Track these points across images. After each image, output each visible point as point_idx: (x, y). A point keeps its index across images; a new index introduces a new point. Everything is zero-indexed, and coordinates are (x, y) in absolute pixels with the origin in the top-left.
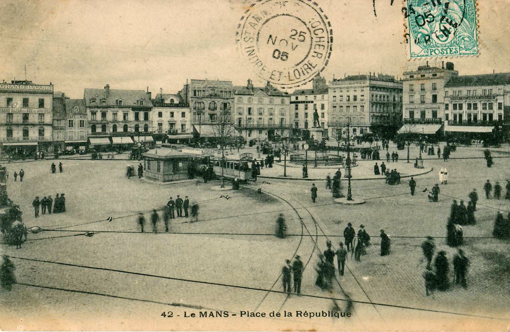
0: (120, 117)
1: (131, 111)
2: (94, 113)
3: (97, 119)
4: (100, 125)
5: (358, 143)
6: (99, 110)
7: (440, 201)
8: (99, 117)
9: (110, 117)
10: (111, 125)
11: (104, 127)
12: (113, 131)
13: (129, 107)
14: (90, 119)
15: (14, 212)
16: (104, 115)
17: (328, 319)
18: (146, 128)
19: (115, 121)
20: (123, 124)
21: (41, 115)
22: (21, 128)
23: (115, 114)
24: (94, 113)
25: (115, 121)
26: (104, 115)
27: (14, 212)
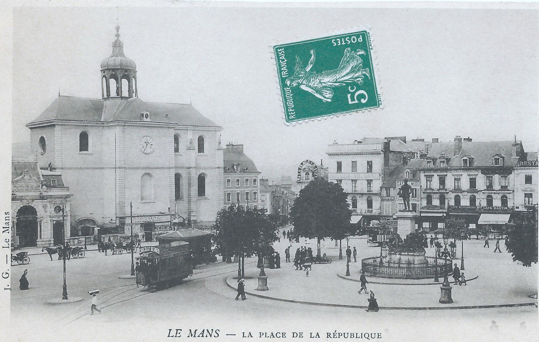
0: (465, 184)
1: (480, 174)
2: (429, 178)
3: (432, 187)
4: (437, 196)
5: (267, 211)
6: (435, 174)
7: (31, 288)
8: (435, 184)
9: (450, 183)
10: (452, 196)
11: (442, 199)
12: (427, 203)
13: (477, 169)
14: (424, 187)
15: (132, 243)
16: (442, 181)
17: (114, 39)
18: (504, 200)
19: (457, 189)
20: (501, 195)
21: (369, 182)
22: (365, 198)
23: (457, 180)
24: (429, 178)
25: (457, 189)
26: (442, 181)
27: (132, 243)
